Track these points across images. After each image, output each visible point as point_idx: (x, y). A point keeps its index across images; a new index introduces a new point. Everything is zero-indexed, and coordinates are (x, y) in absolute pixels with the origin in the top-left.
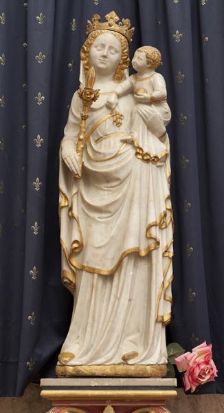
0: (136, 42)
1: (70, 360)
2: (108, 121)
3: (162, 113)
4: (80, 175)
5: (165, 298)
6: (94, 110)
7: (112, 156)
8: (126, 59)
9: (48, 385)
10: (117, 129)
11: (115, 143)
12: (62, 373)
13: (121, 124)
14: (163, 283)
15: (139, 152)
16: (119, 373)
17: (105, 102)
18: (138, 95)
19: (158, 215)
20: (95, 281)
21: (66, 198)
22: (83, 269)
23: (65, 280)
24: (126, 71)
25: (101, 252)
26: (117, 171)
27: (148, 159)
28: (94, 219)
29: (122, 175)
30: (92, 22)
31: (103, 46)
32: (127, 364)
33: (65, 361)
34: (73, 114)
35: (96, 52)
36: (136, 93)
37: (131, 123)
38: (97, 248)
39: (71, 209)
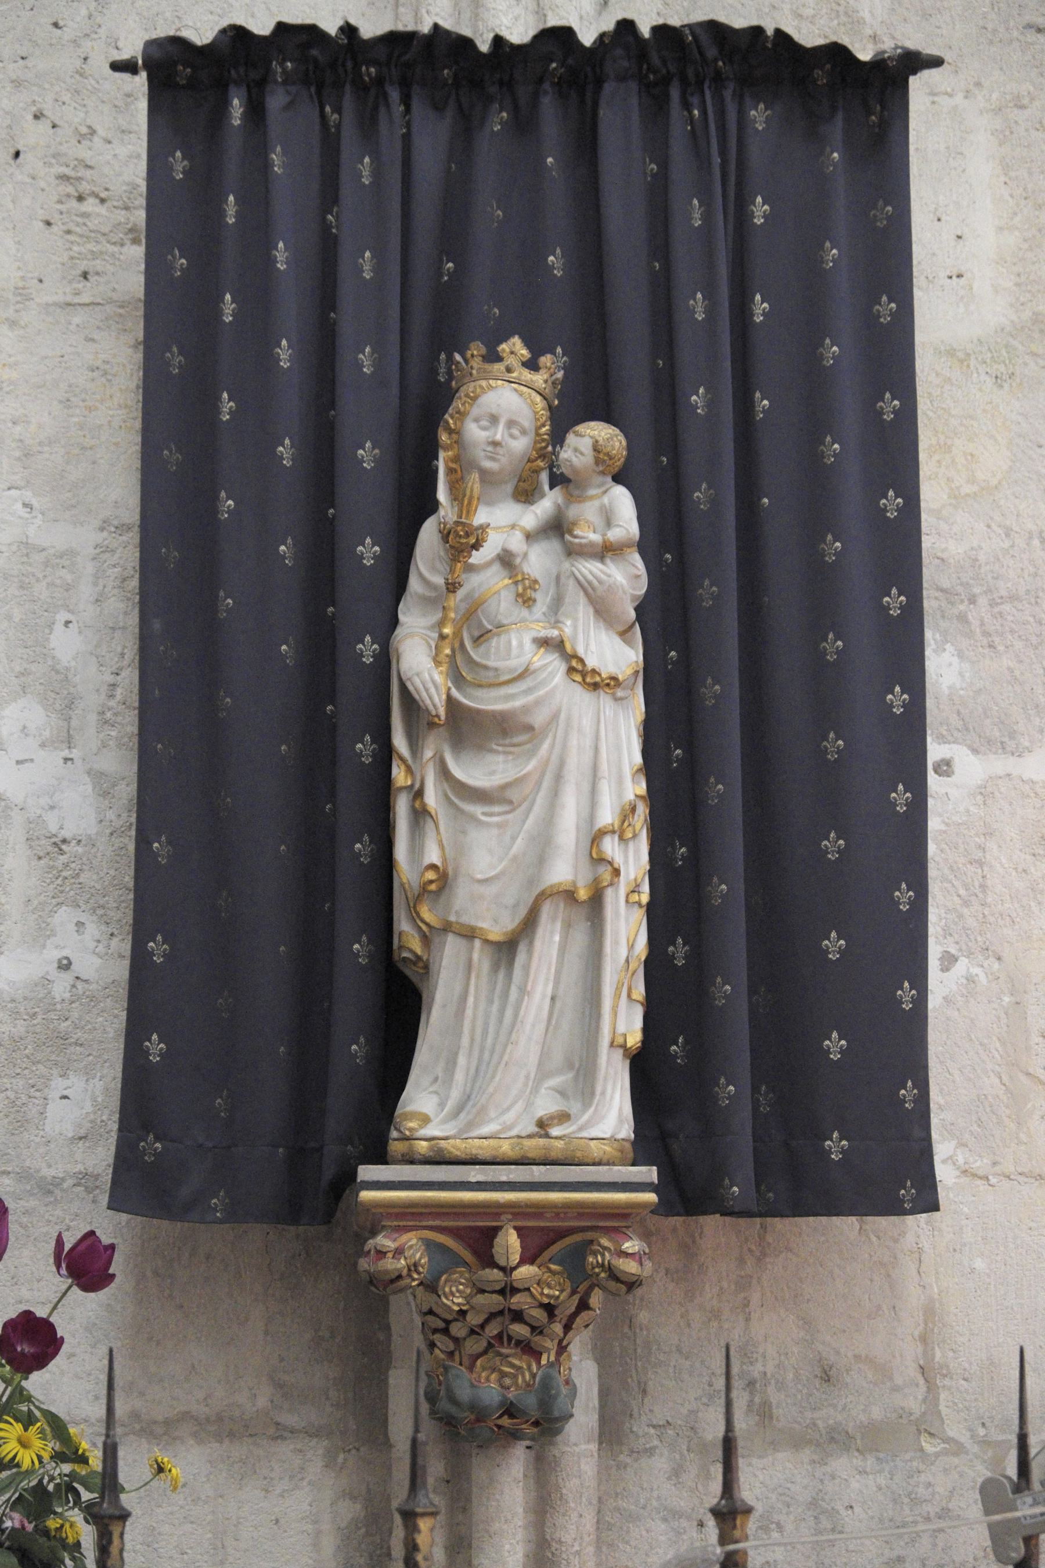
0: (563, 418)
1: (421, 1127)
2: (503, 593)
3: (627, 578)
4: (443, 717)
5: (629, 996)
6: (470, 568)
7: (517, 673)
8: (546, 447)
9: (375, 1179)
10: (525, 613)
11: (521, 645)
12: (403, 1155)
13: (535, 601)
14: (627, 961)
15: (577, 669)
16: (530, 1155)
17: (498, 550)
18: (576, 537)
19: (618, 810)
20: (476, 956)
21: (409, 770)
22: (447, 928)
23: (405, 954)
24: (544, 477)
25: (490, 890)
26: (526, 709)
27: (595, 683)
28: (473, 818)
29: (538, 719)
30: (466, 361)
31: (494, 419)
32: (547, 1136)
33: (411, 1130)
34: (420, 575)
35: (475, 432)
36: (570, 532)
37: (557, 603)
38: (481, 882)
39: (419, 794)
